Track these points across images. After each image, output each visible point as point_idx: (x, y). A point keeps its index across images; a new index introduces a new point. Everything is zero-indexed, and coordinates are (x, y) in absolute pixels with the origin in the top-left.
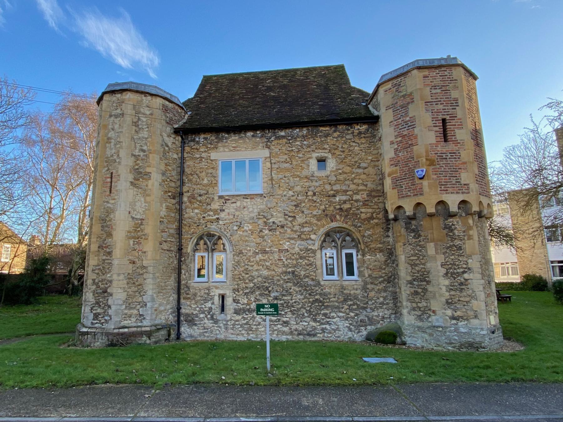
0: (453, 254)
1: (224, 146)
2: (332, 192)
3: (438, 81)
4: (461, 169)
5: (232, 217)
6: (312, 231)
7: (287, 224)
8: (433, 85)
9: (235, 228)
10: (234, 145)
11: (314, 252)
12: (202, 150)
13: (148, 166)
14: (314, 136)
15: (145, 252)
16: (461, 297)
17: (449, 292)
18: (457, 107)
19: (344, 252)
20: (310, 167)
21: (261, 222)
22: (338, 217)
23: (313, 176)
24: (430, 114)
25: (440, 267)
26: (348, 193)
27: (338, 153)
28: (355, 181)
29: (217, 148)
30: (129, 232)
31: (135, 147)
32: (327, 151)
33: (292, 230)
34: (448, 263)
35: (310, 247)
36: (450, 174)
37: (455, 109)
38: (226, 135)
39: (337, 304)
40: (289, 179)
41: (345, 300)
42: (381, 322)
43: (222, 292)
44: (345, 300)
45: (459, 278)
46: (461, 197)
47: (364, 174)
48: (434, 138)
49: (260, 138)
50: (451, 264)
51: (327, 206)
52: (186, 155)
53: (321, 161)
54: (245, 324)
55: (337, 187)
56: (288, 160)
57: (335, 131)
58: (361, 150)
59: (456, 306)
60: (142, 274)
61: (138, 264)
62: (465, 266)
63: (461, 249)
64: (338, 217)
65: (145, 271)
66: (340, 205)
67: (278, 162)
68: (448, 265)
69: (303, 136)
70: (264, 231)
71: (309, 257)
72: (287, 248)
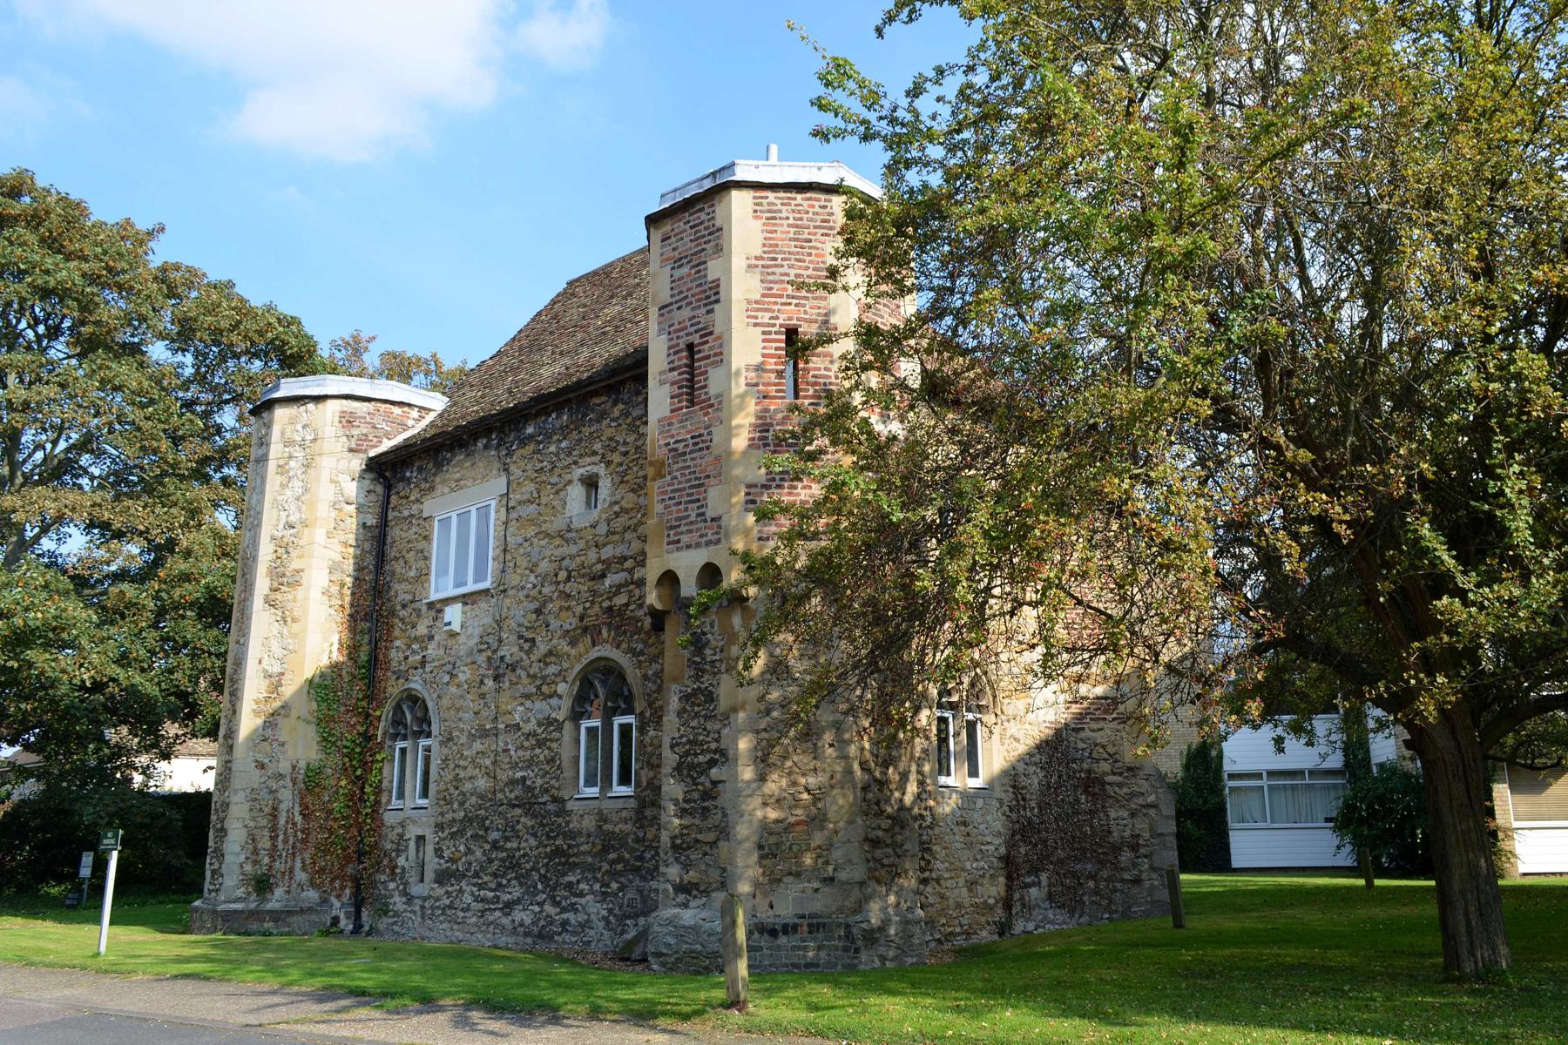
0: (697, 715)
1: (444, 482)
2: (600, 566)
3: (686, 245)
4: (708, 477)
5: (441, 652)
9: (447, 678)
11: (559, 726)
14: (578, 424)
18: (716, 306)
19: (618, 721)
21: (481, 659)
23: (570, 530)
24: (665, 337)
27: (616, 458)
32: (597, 459)
33: (529, 676)
39: (590, 860)
41: (605, 849)
44: (605, 849)
45: (702, 779)
50: (689, 742)
52: (391, 515)
53: (591, 483)
55: (607, 552)
57: (615, 403)
62: (713, 746)
63: (712, 700)
64: (605, 633)
66: (610, 599)
71: (551, 740)
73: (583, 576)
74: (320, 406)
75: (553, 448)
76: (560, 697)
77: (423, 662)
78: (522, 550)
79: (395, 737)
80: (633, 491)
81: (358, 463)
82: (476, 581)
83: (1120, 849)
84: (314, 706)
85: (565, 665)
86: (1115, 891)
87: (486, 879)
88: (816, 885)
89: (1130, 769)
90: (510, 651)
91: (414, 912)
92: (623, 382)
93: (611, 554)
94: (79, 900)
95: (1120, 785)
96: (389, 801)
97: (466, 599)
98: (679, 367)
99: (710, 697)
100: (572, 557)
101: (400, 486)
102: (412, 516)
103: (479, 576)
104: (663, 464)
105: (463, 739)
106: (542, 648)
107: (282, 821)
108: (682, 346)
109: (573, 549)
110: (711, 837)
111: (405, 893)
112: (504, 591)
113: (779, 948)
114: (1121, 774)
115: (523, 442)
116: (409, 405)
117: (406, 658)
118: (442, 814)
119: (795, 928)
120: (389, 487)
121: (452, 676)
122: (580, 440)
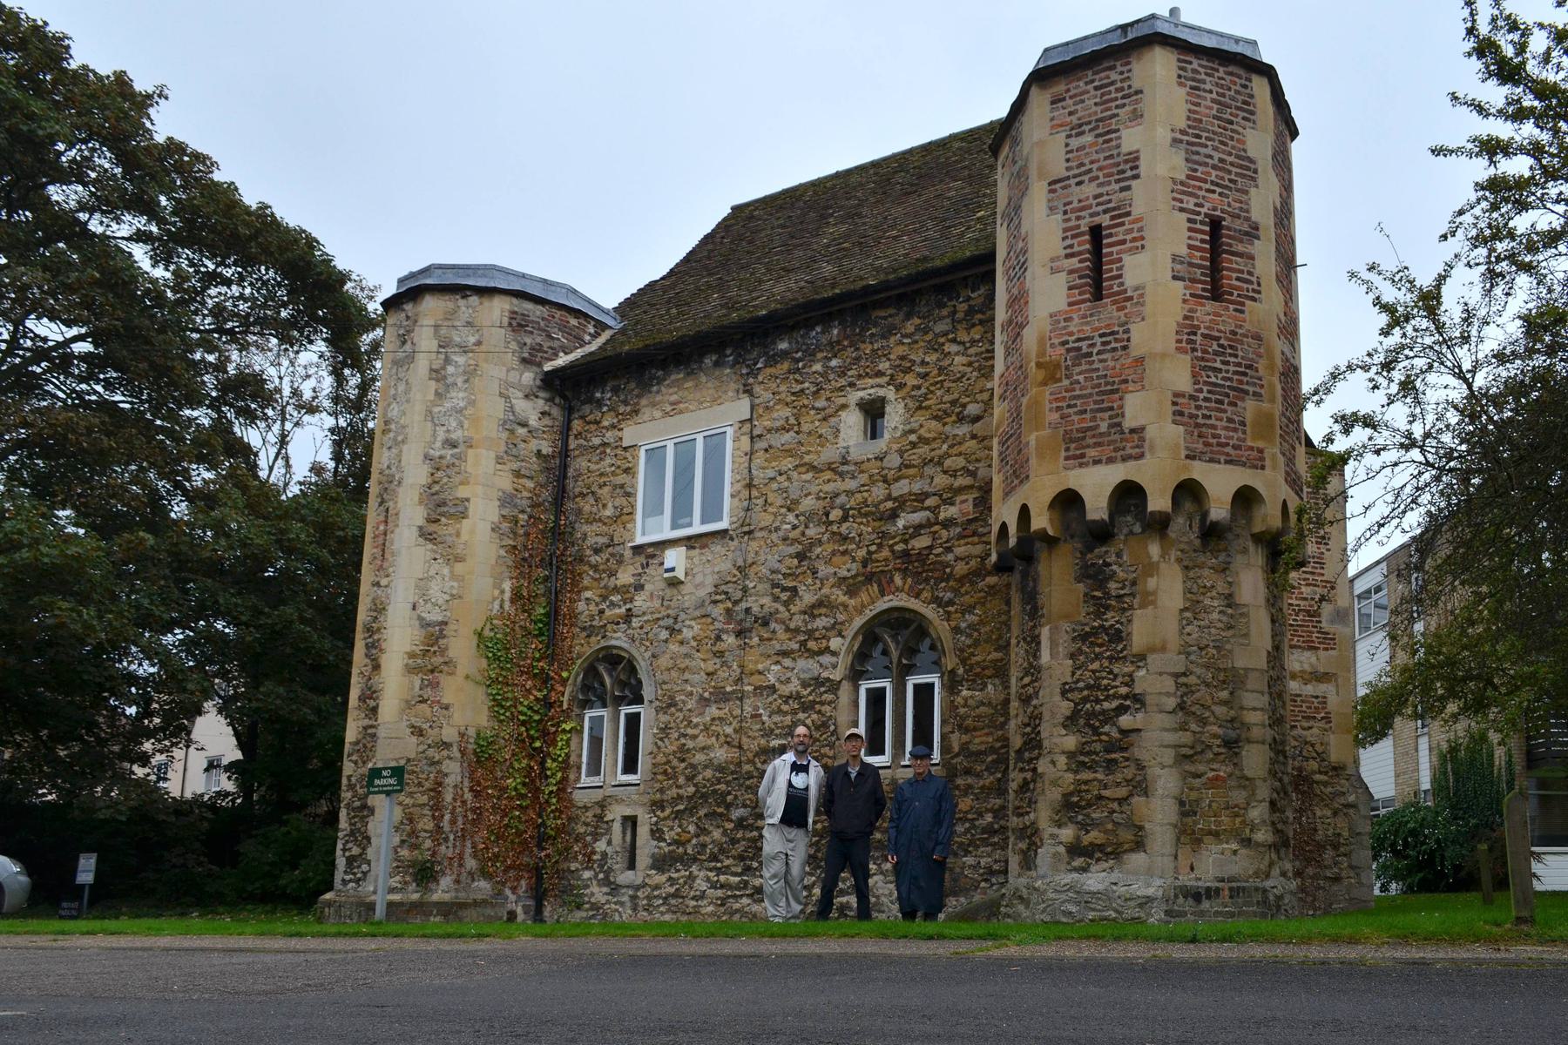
0: (1098, 657)
1: (654, 405)
2: (889, 504)
3: (1090, 106)
4: (1126, 381)
5: (657, 603)
6: (833, 626)
7: (777, 611)
8: (1075, 122)
9: (664, 634)
10: (674, 398)
11: (834, 687)
12: (606, 423)
13: (462, 483)
15: (447, 708)
16: (1105, 787)
17: (1076, 772)
18: (1134, 183)
20: (842, 435)
21: (717, 612)
22: (898, 580)
23: (845, 462)
24: (1060, 217)
25: (1058, 698)
26: (928, 503)
27: (911, 380)
28: (948, 463)
29: (636, 412)
30: (412, 655)
31: (434, 435)
33: (788, 629)
34: (1081, 684)
35: (825, 675)
36: (1096, 402)
37: (1128, 188)
38: (660, 373)
40: (789, 479)
42: (983, 884)
43: (628, 812)
45: (1106, 728)
46: (1114, 474)
47: (974, 437)
48: (1065, 291)
49: (732, 367)
50: (1088, 687)
51: (873, 548)
52: (573, 444)
53: (873, 412)
54: (674, 896)
55: (901, 488)
56: (792, 421)
57: (908, 317)
58: (970, 364)
59: (1088, 816)
60: (439, 762)
61: (432, 734)
62: (1123, 690)
63: (1120, 639)
64: (898, 580)
65: (445, 753)
66: (906, 542)
67: (769, 431)
68: (1081, 690)
69: (831, 343)
70: (724, 637)
71: (822, 703)
72: (773, 681)
73: (866, 515)
74: (486, 302)
75: (818, 367)
76: (834, 654)
77: (629, 615)
78: (775, 486)
79: (586, 704)
80: (936, 418)
81: (529, 377)
82: (703, 522)
83: (1324, 847)
84: (484, 663)
85: (841, 617)
86: (1319, 888)
87: (727, 862)
88: (1234, 846)
89: (1335, 769)
90: (760, 602)
91: (622, 904)
92: (919, 292)
93: (906, 490)
94: (79, 910)
95: (1325, 784)
96: (578, 779)
97: (690, 542)
98: (1080, 253)
99: (1117, 636)
100: (849, 493)
101: (587, 408)
102: (605, 444)
103: (711, 513)
104: (1058, 366)
105: (691, 704)
106: (808, 598)
107: (448, 798)
108: (1084, 229)
109: (851, 484)
110: (1122, 792)
111: (606, 882)
112: (750, 532)
113: (1202, 914)
114: (1326, 773)
115: (773, 360)
116: (586, 316)
117: (602, 612)
118: (662, 791)
119: (1217, 891)
120: (569, 411)
121: (672, 631)
122: (858, 359)
